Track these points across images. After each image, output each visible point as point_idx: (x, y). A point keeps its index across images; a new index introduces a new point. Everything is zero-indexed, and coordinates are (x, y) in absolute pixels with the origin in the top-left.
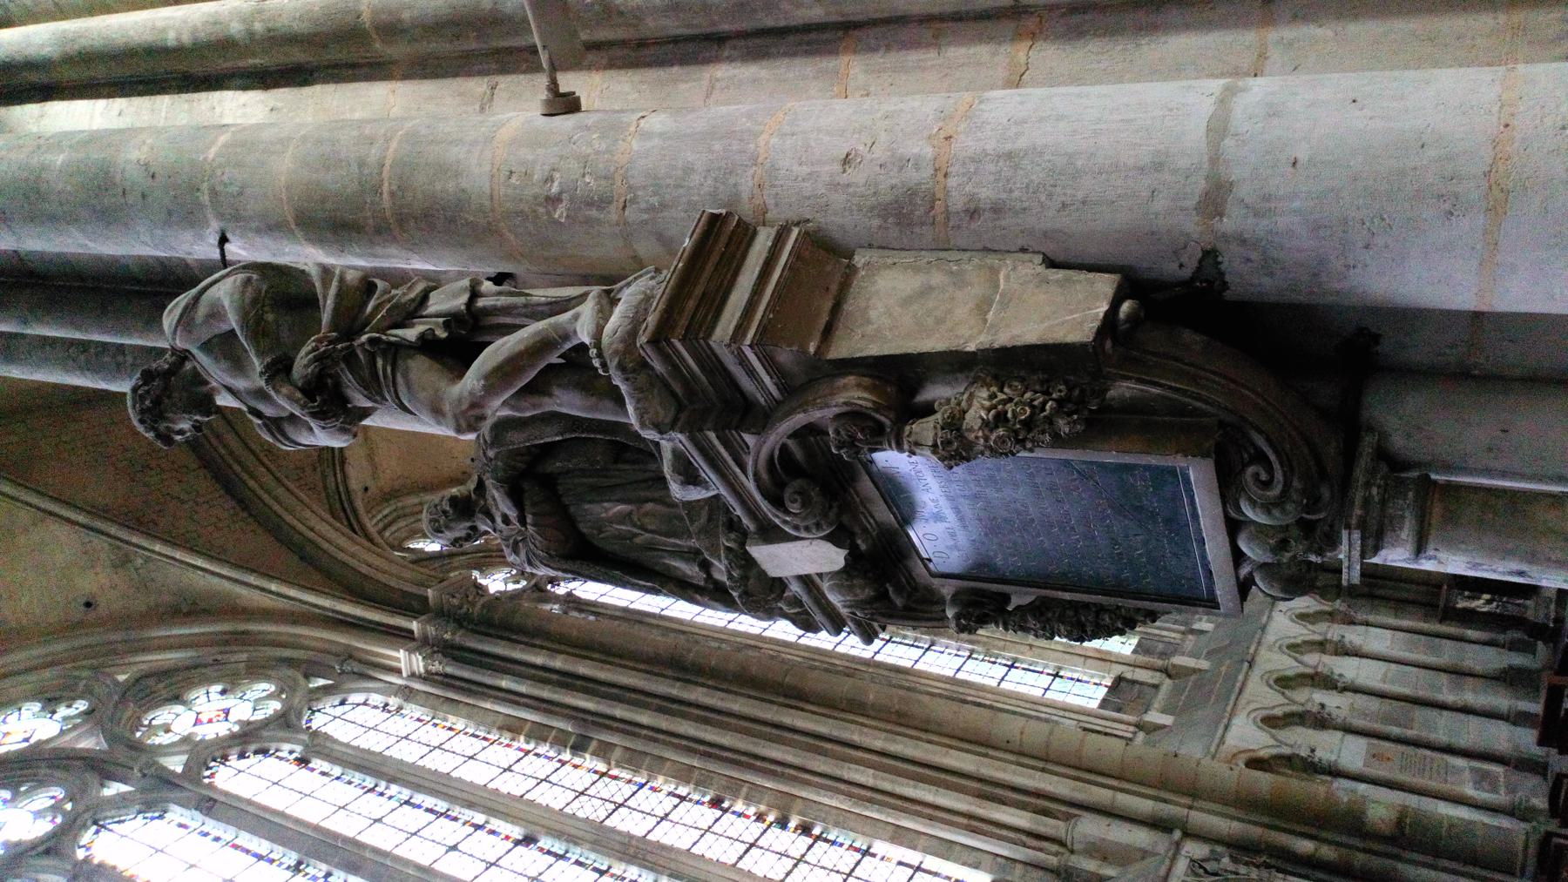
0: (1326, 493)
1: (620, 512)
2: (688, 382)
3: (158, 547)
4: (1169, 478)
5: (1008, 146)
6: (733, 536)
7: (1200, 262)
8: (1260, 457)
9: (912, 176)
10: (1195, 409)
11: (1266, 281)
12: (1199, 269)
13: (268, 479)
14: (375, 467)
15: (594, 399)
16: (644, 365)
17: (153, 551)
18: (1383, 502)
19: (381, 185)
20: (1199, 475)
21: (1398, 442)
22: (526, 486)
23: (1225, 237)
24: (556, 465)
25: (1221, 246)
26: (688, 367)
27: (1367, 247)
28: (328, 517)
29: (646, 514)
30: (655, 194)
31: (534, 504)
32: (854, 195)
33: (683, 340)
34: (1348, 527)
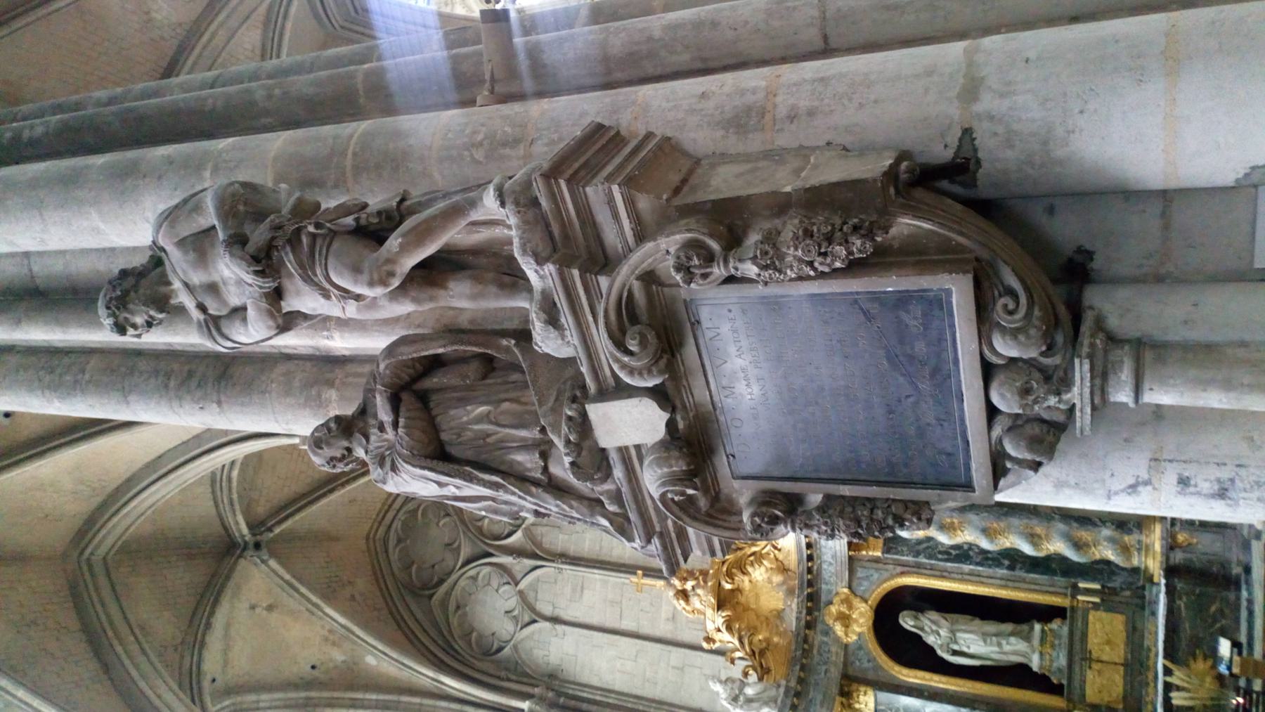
0: (1060, 339)
1: (481, 414)
3: (21, 693)
4: (937, 304)
5: (821, 75)
6: (574, 406)
7: (960, 140)
8: (1011, 293)
9: (750, 99)
10: (958, 244)
11: (1009, 154)
12: (959, 147)
13: (134, 648)
14: (226, 663)
15: (480, 287)
16: (535, 203)
17: (14, 696)
18: (1106, 352)
20: (958, 292)
21: (1113, 322)
22: (405, 396)
23: (979, 117)
25: (975, 125)
26: (567, 210)
27: (1081, 112)
28: (175, 687)
29: (502, 413)
30: (556, 131)
32: (705, 116)
33: (568, 181)
34: (1079, 356)
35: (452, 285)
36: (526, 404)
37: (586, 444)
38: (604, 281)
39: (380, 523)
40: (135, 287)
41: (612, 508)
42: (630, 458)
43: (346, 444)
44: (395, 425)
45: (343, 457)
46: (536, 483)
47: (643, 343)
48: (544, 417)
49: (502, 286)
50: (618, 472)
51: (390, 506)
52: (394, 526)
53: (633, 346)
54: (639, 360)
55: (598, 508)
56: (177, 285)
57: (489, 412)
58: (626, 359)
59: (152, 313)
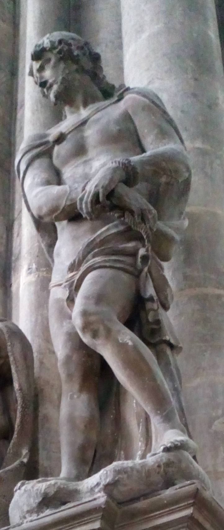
2: (146, 514)
15: (82, 426)
16: (169, 483)
26: (161, 516)
33: (191, 518)
35: (84, 397)
40: (82, 70)
56: (84, 113)
59: (55, 87)
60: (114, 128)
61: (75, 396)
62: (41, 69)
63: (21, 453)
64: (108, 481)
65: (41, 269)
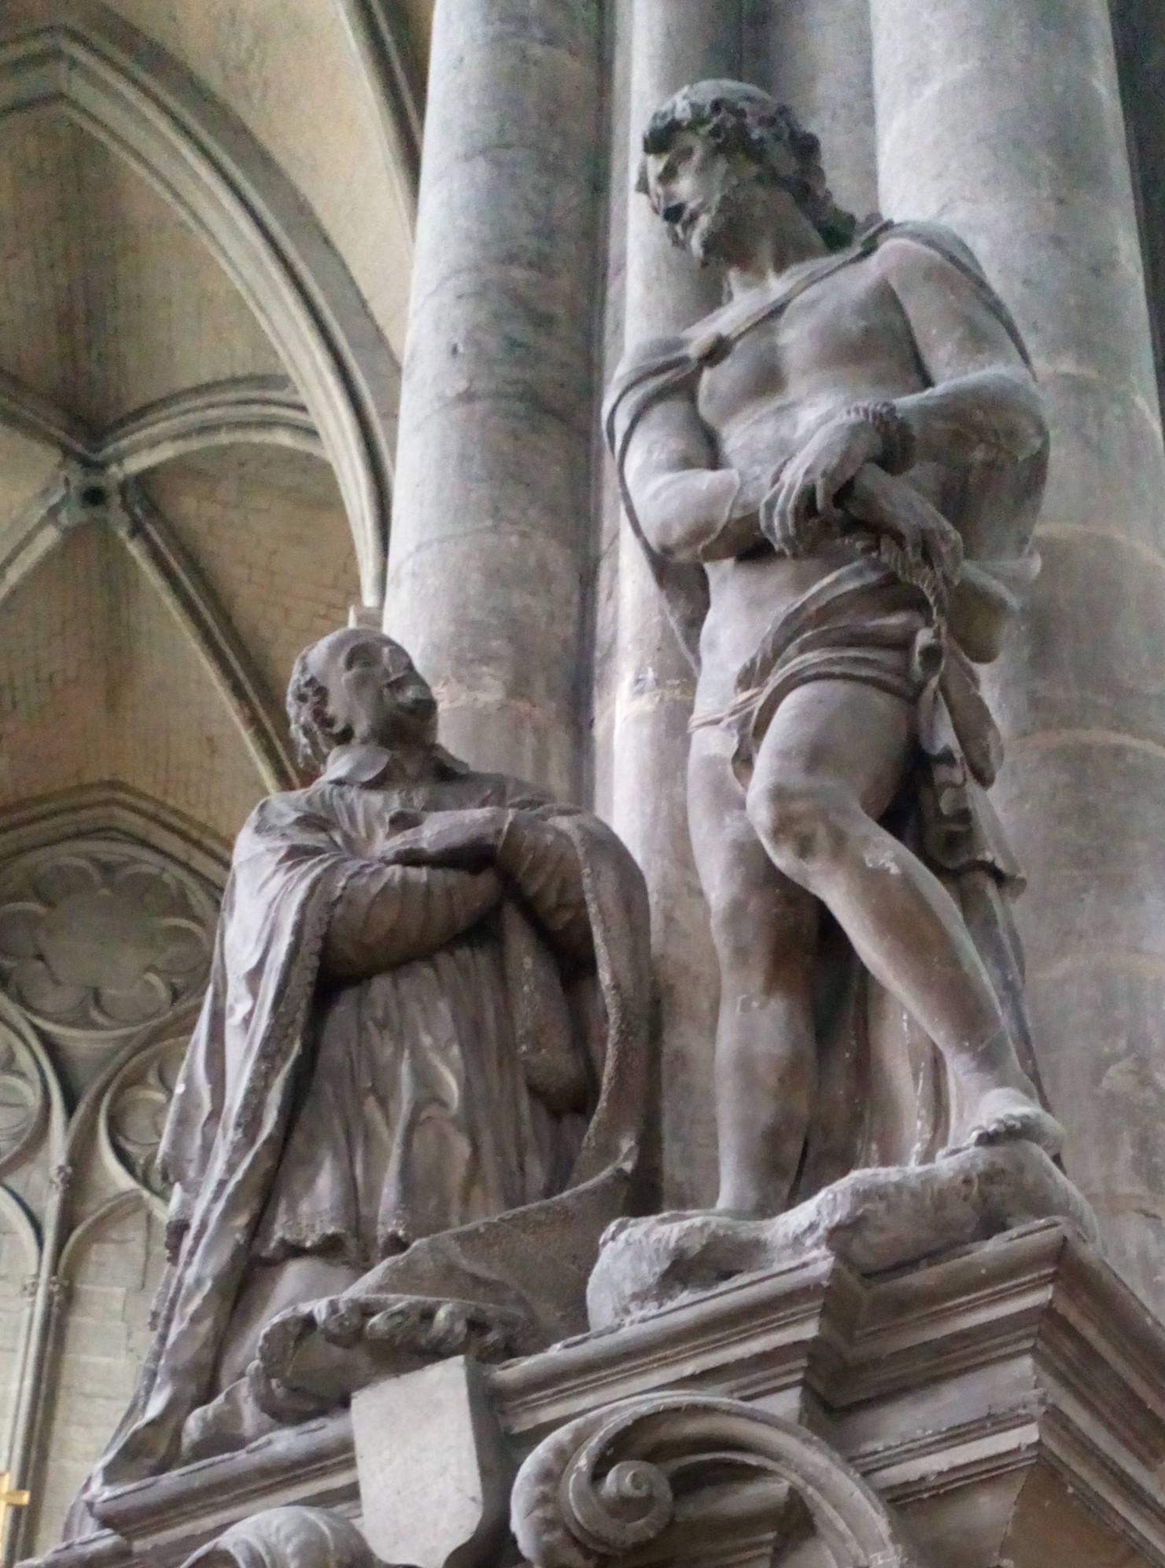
2: (932, 1301)
6: (460, 1327)
15: (772, 1080)
16: (992, 1224)
19: (1130, 731)
24: (525, 957)
26: (972, 1307)
29: (442, 1138)
31: (449, 893)
33: (1047, 1312)
35: (778, 1006)
36: (466, 1200)
37: (360, 1358)
38: (786, 1403)
39: (153, 818)
40: (772, 178)
41: (193, 1425)
42: (323, 1472)
43: (361, 728)
44: (410, 858)
45: (327, 723)
46: (258, 1227)
47: (623, 1507)
48: (433, 1249)
49: (774, 1137)
50: (286, 1442)
51: (198, 844)
52: (146, 855)
53: (618, 1480)
54: (581, 1496)
55: (192, 1389)
56: (777, 286)
57: (444, 1104)
58: (583, 1462)
59: (704, 221)
60: (853, 325)
61: (755, 1004)
62: (668, 175)
63: (618, 1149)
64: (837, 1218)
65: (669, 682)
